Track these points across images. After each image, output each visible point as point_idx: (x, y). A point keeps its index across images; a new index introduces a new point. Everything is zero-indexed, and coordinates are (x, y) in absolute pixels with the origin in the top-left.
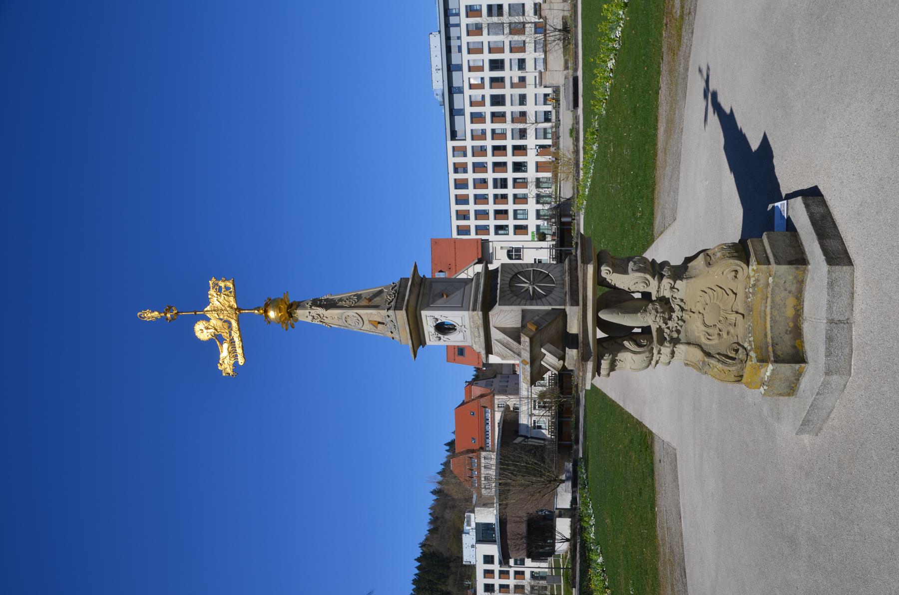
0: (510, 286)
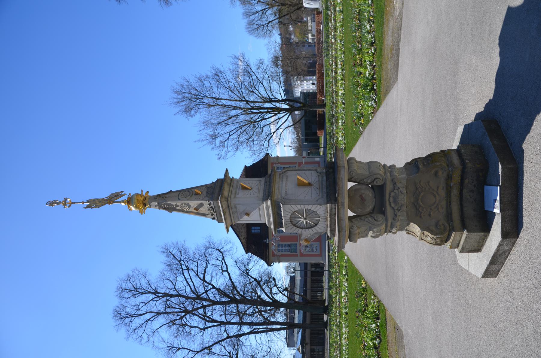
0: (291, 222)
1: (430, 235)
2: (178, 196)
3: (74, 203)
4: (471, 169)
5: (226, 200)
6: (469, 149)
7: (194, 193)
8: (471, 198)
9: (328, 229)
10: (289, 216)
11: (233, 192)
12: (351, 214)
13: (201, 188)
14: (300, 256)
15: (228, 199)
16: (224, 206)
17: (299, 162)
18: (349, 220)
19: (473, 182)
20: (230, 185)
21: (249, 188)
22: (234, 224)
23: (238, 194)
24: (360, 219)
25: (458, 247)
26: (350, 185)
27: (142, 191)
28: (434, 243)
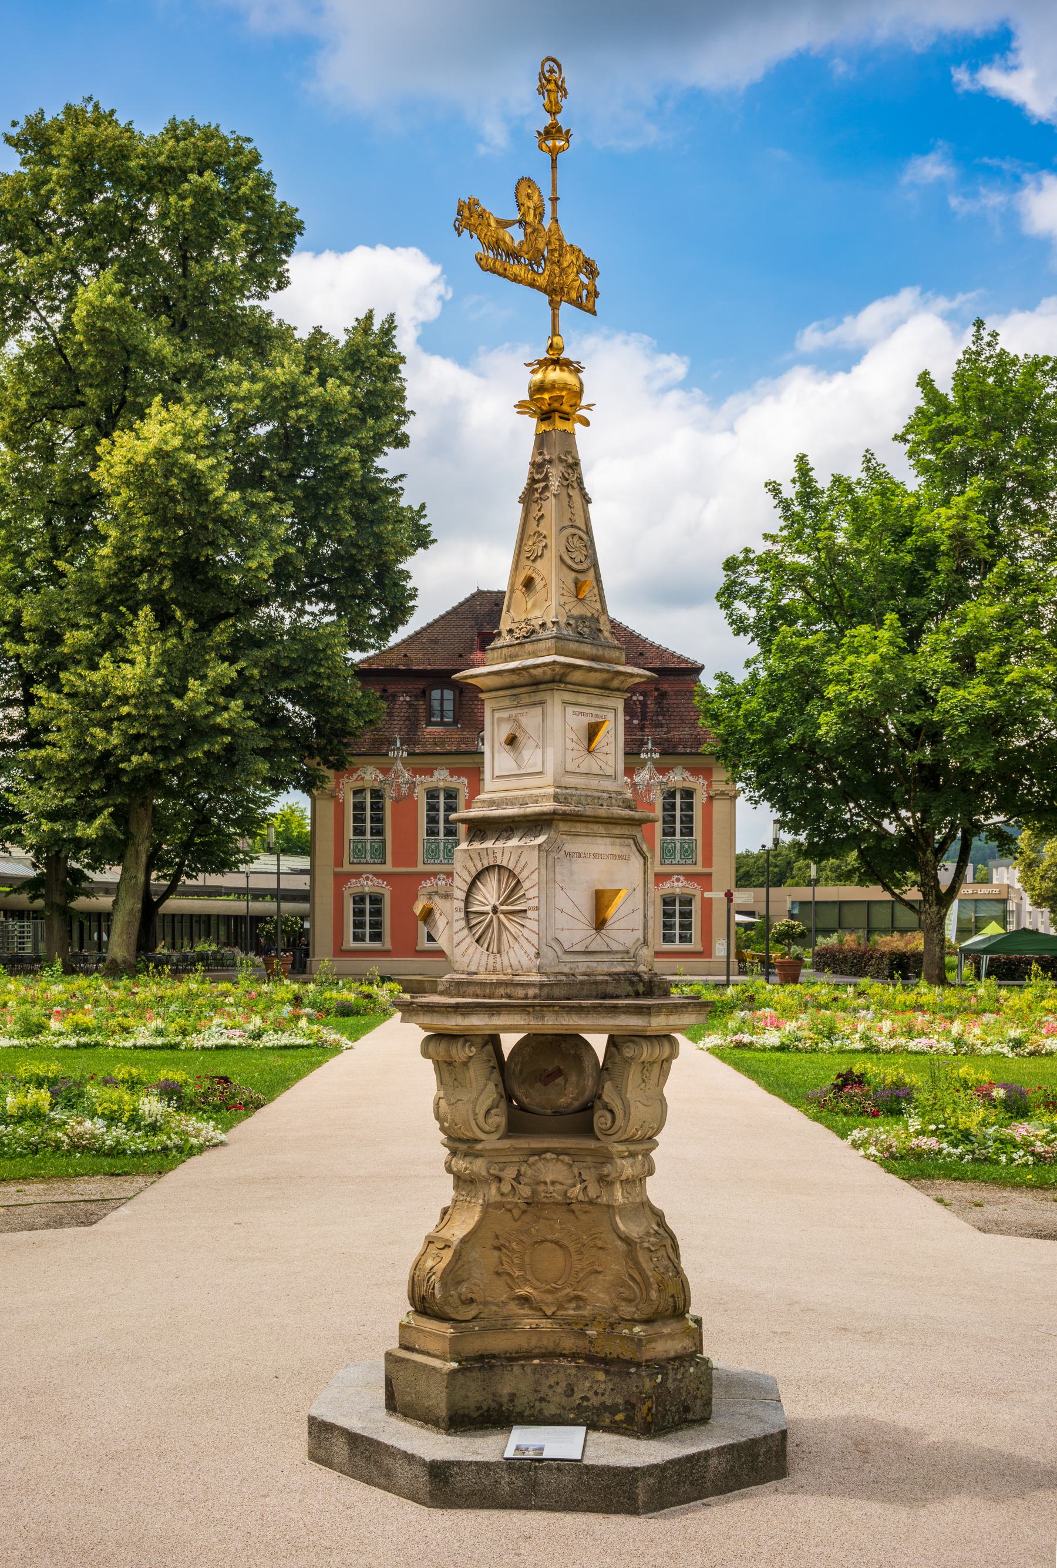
1: (443, 1265)
2: (572, 526)
3: (554, 167)
4: (634, 1388)
5: (558, 678)
6: (698, 1389)
7: (580, 576)
8: (551, 1387)
9: (464, 976)
10: (504, 864)
11: (582, 699)
12: (509, 1042)
13: (597, 598)
14: (336, 875)
15: (560, 682)
16: (540, 670)
17: (710, 875)
18: (491, 1035)
19: (596, 1393)
20: (602, 688)
21: (593, 745)
22: (482, 696)
23: (574, 713)
24: (494, 1068)
25: (404, 1347)
26: (598, 1043)
27: (588, 407)
28: (416, 1278)
